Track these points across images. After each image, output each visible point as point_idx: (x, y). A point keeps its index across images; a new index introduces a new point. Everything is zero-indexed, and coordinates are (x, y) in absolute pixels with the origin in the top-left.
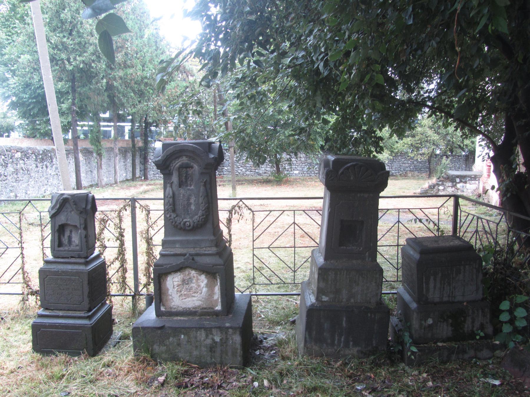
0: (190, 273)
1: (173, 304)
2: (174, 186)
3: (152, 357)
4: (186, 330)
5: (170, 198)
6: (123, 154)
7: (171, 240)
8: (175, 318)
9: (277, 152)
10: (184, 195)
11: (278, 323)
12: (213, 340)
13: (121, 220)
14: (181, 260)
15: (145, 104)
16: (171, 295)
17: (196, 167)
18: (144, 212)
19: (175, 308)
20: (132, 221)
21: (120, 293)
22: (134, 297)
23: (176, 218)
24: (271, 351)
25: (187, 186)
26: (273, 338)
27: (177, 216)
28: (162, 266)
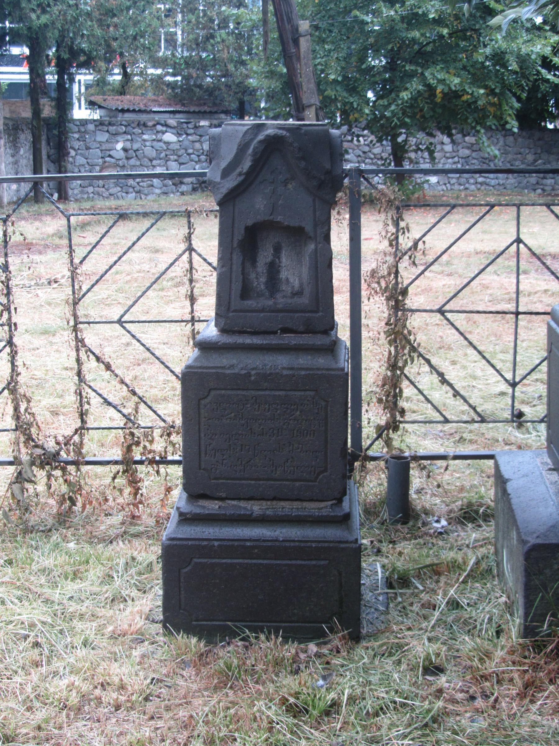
6: (9, 135)
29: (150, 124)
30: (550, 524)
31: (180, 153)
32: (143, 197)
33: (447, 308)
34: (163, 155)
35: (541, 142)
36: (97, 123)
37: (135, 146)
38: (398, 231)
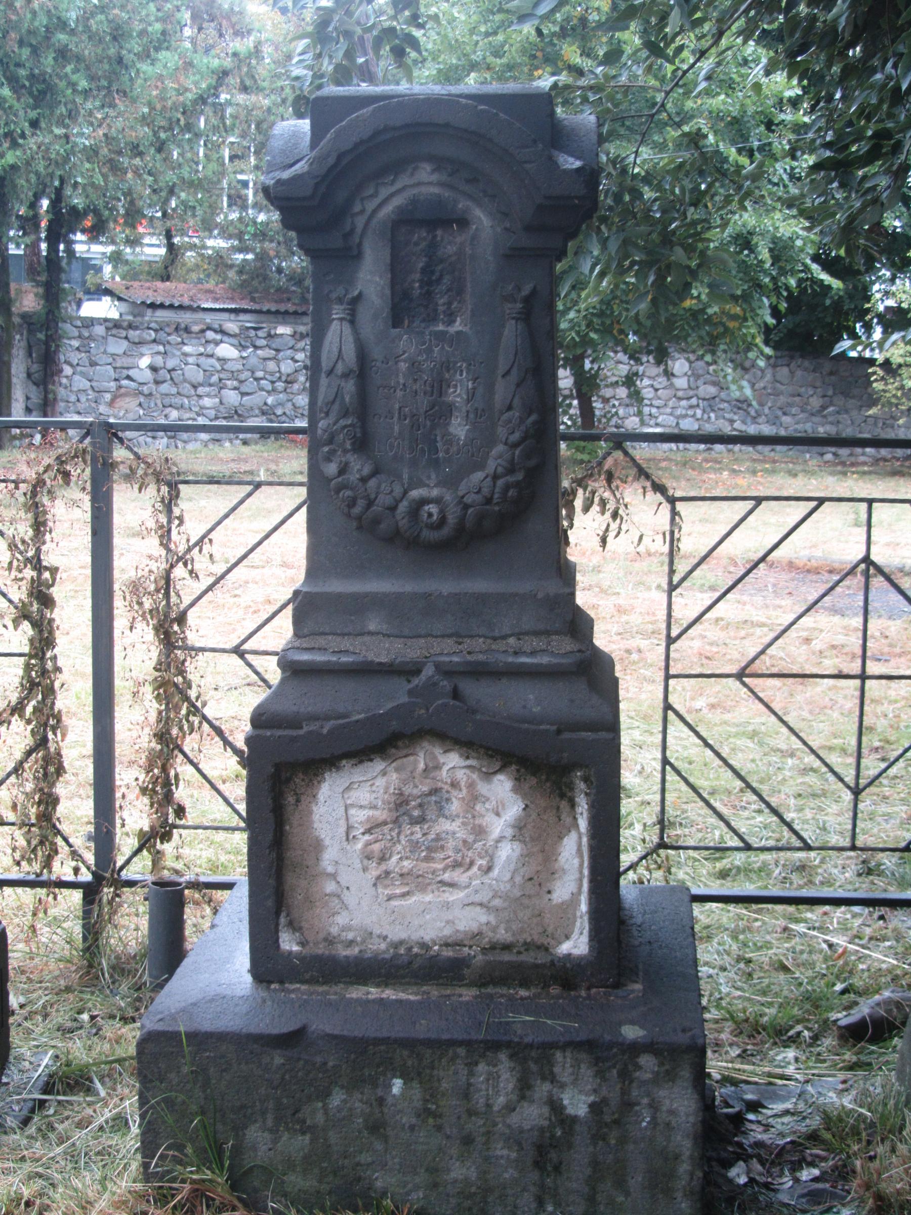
0: (438, 767)
1: (342, 919)
2: (364, 314)
3: (235, 1185)
4: (415, 1054)
5: (346, 376)
7: (339, 596)
8: (356, 993)
9: (586, 342)
10: (414, 364)
11: (781, 1035)
12: (556, 1107)
13: (40, 526)
14: (395, 695)
15: (58, 131)
16: (334, 876)
17: (483, 220)
18: (151, 490)
19: (351, 943)
20: (94, 533)
21: (29, 870)
22: (91, 892)
23: (372, 483)
24: (796, 1167)
25: (432, 318)
26: (788, 1105)
27: (375, 473)
28: (293, 722)
29: (196, 328)
30: (190, 1001)
31: (243, 377)
32: (180, 444)
33: (246, 647)
34: (214, 379)
35: (833, 378)
36: (110, 325)
37: (171, 364)
38: (170, 522)
